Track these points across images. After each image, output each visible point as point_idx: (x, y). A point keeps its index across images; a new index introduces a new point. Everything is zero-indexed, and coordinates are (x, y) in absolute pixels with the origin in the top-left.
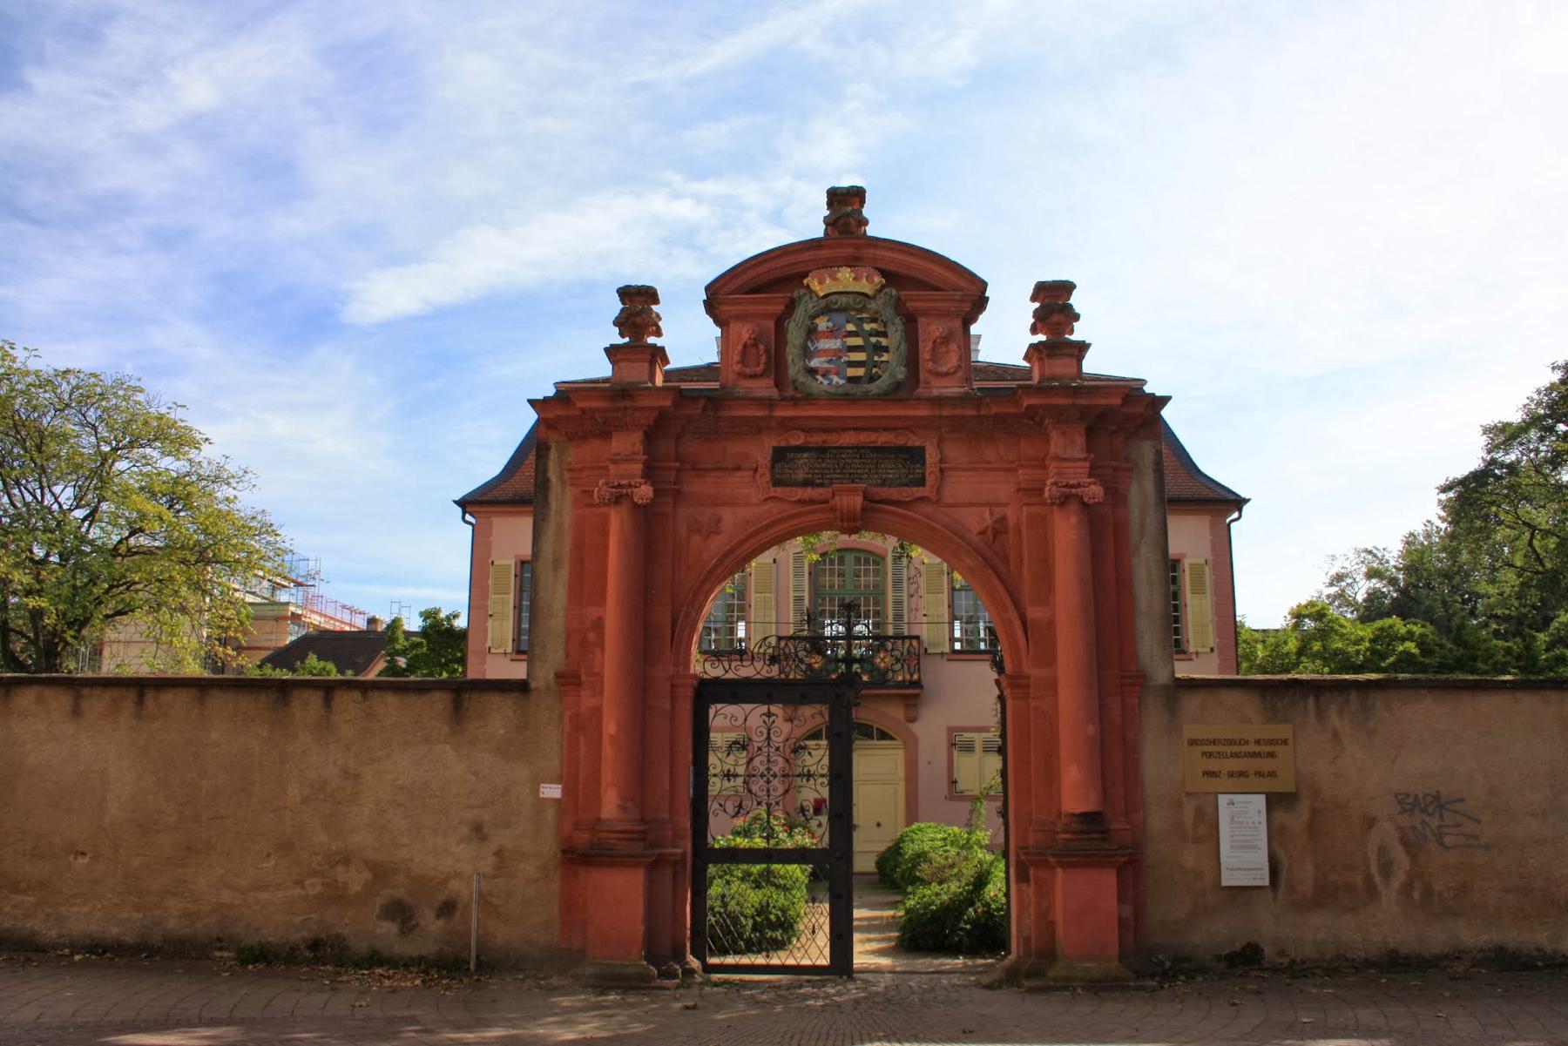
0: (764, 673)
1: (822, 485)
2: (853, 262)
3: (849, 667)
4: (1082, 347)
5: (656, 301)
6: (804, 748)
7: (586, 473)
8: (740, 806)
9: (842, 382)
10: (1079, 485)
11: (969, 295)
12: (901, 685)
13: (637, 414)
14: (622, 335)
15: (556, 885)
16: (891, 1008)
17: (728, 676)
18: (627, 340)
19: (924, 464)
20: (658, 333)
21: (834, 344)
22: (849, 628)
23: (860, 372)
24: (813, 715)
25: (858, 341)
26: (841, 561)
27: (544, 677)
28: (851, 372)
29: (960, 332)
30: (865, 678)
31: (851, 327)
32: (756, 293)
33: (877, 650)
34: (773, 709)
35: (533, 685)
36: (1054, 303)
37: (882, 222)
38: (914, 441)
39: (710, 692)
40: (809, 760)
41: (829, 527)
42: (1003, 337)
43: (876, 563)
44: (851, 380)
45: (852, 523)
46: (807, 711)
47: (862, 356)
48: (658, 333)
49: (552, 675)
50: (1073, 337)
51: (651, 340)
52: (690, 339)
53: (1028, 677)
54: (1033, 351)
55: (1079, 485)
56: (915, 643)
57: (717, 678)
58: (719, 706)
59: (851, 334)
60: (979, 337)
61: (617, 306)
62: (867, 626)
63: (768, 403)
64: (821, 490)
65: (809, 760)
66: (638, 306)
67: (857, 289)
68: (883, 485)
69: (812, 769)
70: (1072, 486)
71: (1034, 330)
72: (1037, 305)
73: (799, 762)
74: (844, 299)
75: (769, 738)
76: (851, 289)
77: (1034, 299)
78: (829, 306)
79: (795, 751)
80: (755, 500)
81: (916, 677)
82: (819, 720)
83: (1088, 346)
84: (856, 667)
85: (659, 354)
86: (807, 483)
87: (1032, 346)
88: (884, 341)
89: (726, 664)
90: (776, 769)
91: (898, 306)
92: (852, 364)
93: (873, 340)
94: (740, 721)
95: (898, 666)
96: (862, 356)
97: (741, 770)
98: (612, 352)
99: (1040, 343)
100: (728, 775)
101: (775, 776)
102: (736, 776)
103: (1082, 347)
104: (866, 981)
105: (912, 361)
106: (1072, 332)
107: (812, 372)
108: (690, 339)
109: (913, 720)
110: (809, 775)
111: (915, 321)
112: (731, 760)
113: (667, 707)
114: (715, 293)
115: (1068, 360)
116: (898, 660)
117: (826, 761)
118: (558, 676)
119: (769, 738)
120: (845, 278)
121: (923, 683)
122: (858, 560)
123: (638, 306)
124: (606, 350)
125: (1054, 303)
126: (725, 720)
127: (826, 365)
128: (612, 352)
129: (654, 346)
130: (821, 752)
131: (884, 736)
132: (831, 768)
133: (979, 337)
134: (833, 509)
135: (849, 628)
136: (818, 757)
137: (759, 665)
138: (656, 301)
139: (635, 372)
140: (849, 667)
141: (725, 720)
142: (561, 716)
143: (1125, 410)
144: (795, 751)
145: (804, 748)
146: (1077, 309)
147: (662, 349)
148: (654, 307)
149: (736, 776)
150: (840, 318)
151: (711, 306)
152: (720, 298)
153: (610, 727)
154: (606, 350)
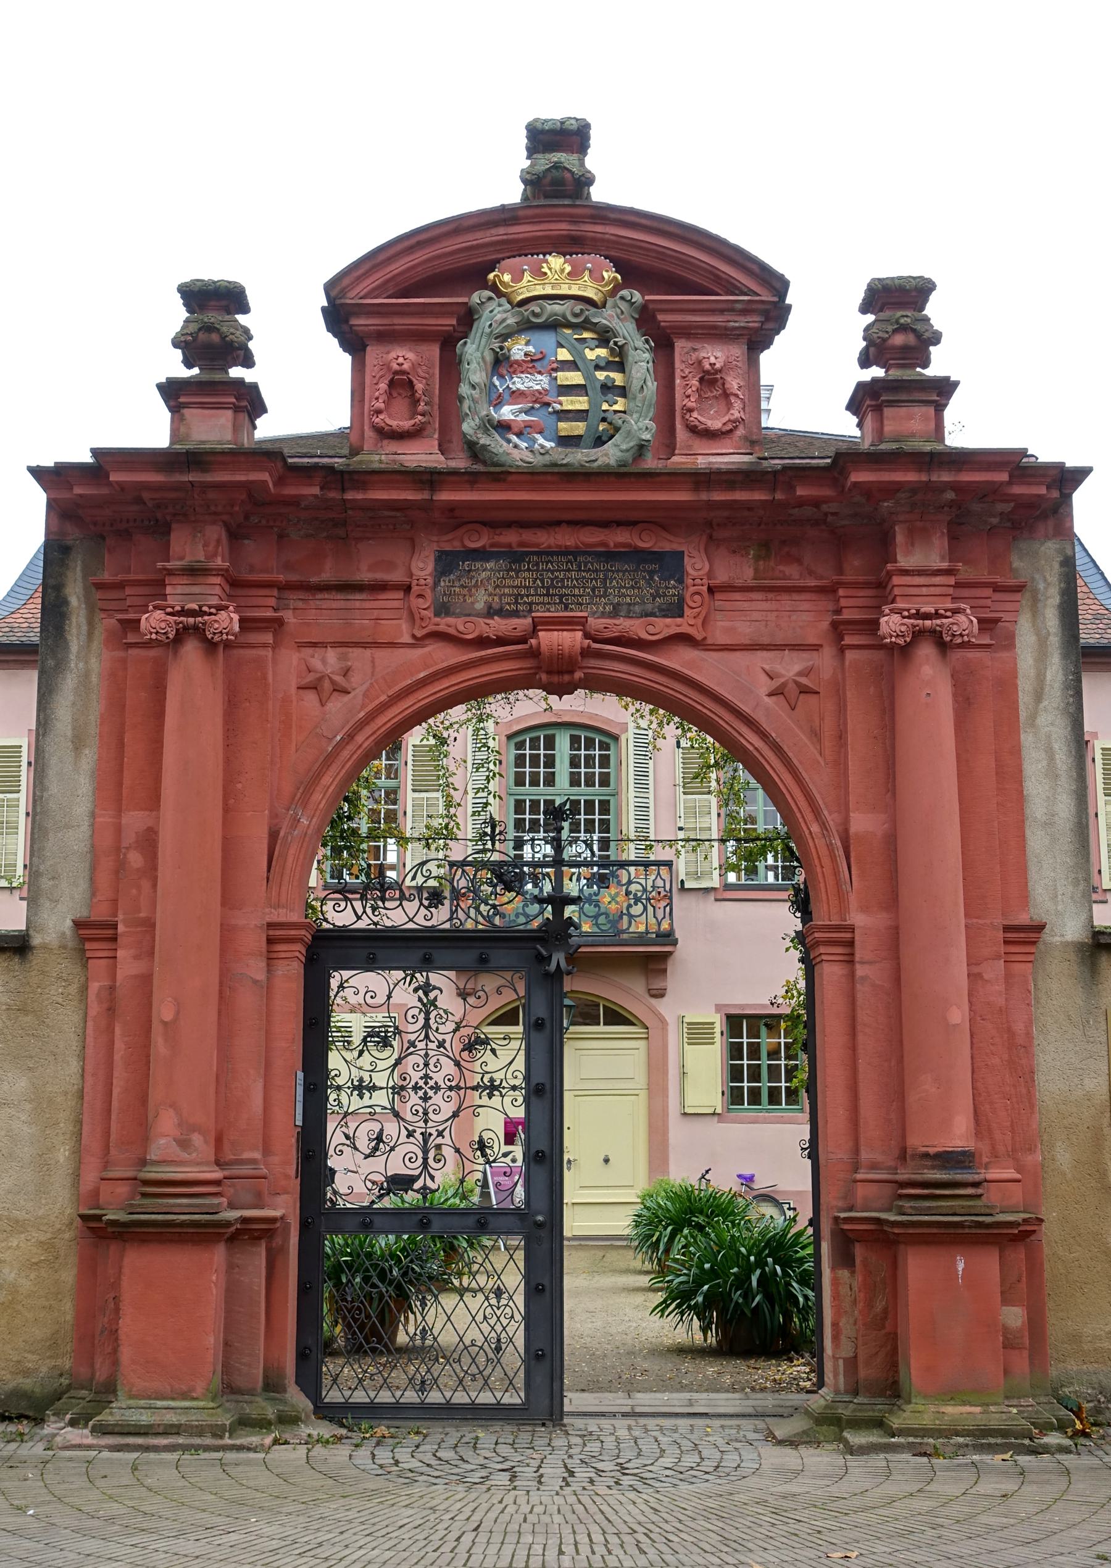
0: (420, 920)
1: (515, 614)
2: (569, 245)
3: (558, 911)
4: (945, 388)
5: (245, 309)
6: (486, 1042)
7: (128, 591)
8: (379, 1139)
9: (549, 445)
10: (937, 615)
11: (756, 304)
12: (641, 939)
13: (212, 495)
14: (188, 364)
15: (68, 1276)
16: (626, 1481)
17: (361, 925)
18: (196, 371)
19: (681, 581)
20: (248, 361)
21: (537, 382)
22: (558, 848)
23: (578, 428)
24: (501, 990)
25: (575, 378)
26: (550, 743)
27: (56, 925)
28: (566, 428)
29: (742, 364)
30: (586, 928)
31: (564, 355)
32: (411, 299)
33: (602, 881)
34: (435, 978)
35: (36, 940)
36: (898, 314)
37: (616, 179)
38: (667, 545)
39: (329, 951)
40: (493, 1064)
41: (525, 682)
42: (809, 386)
43: (604, 746)
44: (568, 441)
45: (559, 676)
46: (489, 982)
47: (580, 403)
48: (248, 361)
49: (69, 923)
50: (931, 372)
51: (236, 372)
52: (305, 389)
53: (851, 929)
54: (864, 401)
55: (937, 615)
56: (664, 871)
57: (344, 929)
58: (346, 974)
59: (565, 365)
60: (770, 388)
61: (177, 315)
62: (589, 846)
63: (429, 479)
64: (515, 621)
65: (493, 1064)
66: (214, 321)
67: (575, 291)
68: (615, 614)
69: (498, 1076)
70: (927, 616)
71: (865, 361)
72: (870, 318)
73: (477, 1066)
74: (557, 308)
75: (427, 1026)
76: (564, 290)
77: (865, 309)
78: (533, 320)
79: (469, 1047)
80: (407, 639)
81: (665, 926)
82: (509, 996)
83: (956, 384)
84: (569, 911)
85: (250, 402)
86: (490, 612)
87: (861, 387)
88: (618, 378)
89: (358, 905)
90: (414, 1099)
91: (645, 319)
92: (564, 415)
93: (601, 375)
94: (381, 999)
95: (637, 909)
96: (580, 403)
97: (380, 1079)
98: (171, 391)
99: (875, 381)
100: (361, 1088)
101: (436, 1088)
102: (374, 1088)
103: (945, 388)
104: (586, 1436)
105: (666, 411)
106: (926, 364)
107: (504, 427)
108: (305, 389)
109: (660, 994)
110: (492, 1088)
111: (671, 346)
112: (366, 1060)
113: (261, 976)
114: (343, 293)
115: (919, 411)
116: (637, 900)
117: (520, 1064)
118: (78, 924)
119: (427, 1026)
120: (556, 275)
121: (678, 934)
122: (575, 741)
123: (214, 321)
124: (160, 387)
125: (898, 314)
126: (363, 997)
127: (523, 417)
128: (171, 391)
129: (240, 382)
130: (515, 1044)
131: (616, 1017)
132: (527, 1078)
133: (770, 388)
134: (535, 653)
135: (558, 848)
136: (507, 1058)
137: (411, 907)
138: (245, 309)
139: (213, 429)
140: (558, 911)
141: (363, 997)
142: (84, 989)
143: (1017, 490)
144: (469, 1047)
145: (486, 1042)
146: (937, 324)
147: (254, 387)
148: (241, 319)
149: (374, 1088)
150: (547, 340)
151: (338, 317)
152: (348, 314)
153: (826, 813)
154: (160, 387)
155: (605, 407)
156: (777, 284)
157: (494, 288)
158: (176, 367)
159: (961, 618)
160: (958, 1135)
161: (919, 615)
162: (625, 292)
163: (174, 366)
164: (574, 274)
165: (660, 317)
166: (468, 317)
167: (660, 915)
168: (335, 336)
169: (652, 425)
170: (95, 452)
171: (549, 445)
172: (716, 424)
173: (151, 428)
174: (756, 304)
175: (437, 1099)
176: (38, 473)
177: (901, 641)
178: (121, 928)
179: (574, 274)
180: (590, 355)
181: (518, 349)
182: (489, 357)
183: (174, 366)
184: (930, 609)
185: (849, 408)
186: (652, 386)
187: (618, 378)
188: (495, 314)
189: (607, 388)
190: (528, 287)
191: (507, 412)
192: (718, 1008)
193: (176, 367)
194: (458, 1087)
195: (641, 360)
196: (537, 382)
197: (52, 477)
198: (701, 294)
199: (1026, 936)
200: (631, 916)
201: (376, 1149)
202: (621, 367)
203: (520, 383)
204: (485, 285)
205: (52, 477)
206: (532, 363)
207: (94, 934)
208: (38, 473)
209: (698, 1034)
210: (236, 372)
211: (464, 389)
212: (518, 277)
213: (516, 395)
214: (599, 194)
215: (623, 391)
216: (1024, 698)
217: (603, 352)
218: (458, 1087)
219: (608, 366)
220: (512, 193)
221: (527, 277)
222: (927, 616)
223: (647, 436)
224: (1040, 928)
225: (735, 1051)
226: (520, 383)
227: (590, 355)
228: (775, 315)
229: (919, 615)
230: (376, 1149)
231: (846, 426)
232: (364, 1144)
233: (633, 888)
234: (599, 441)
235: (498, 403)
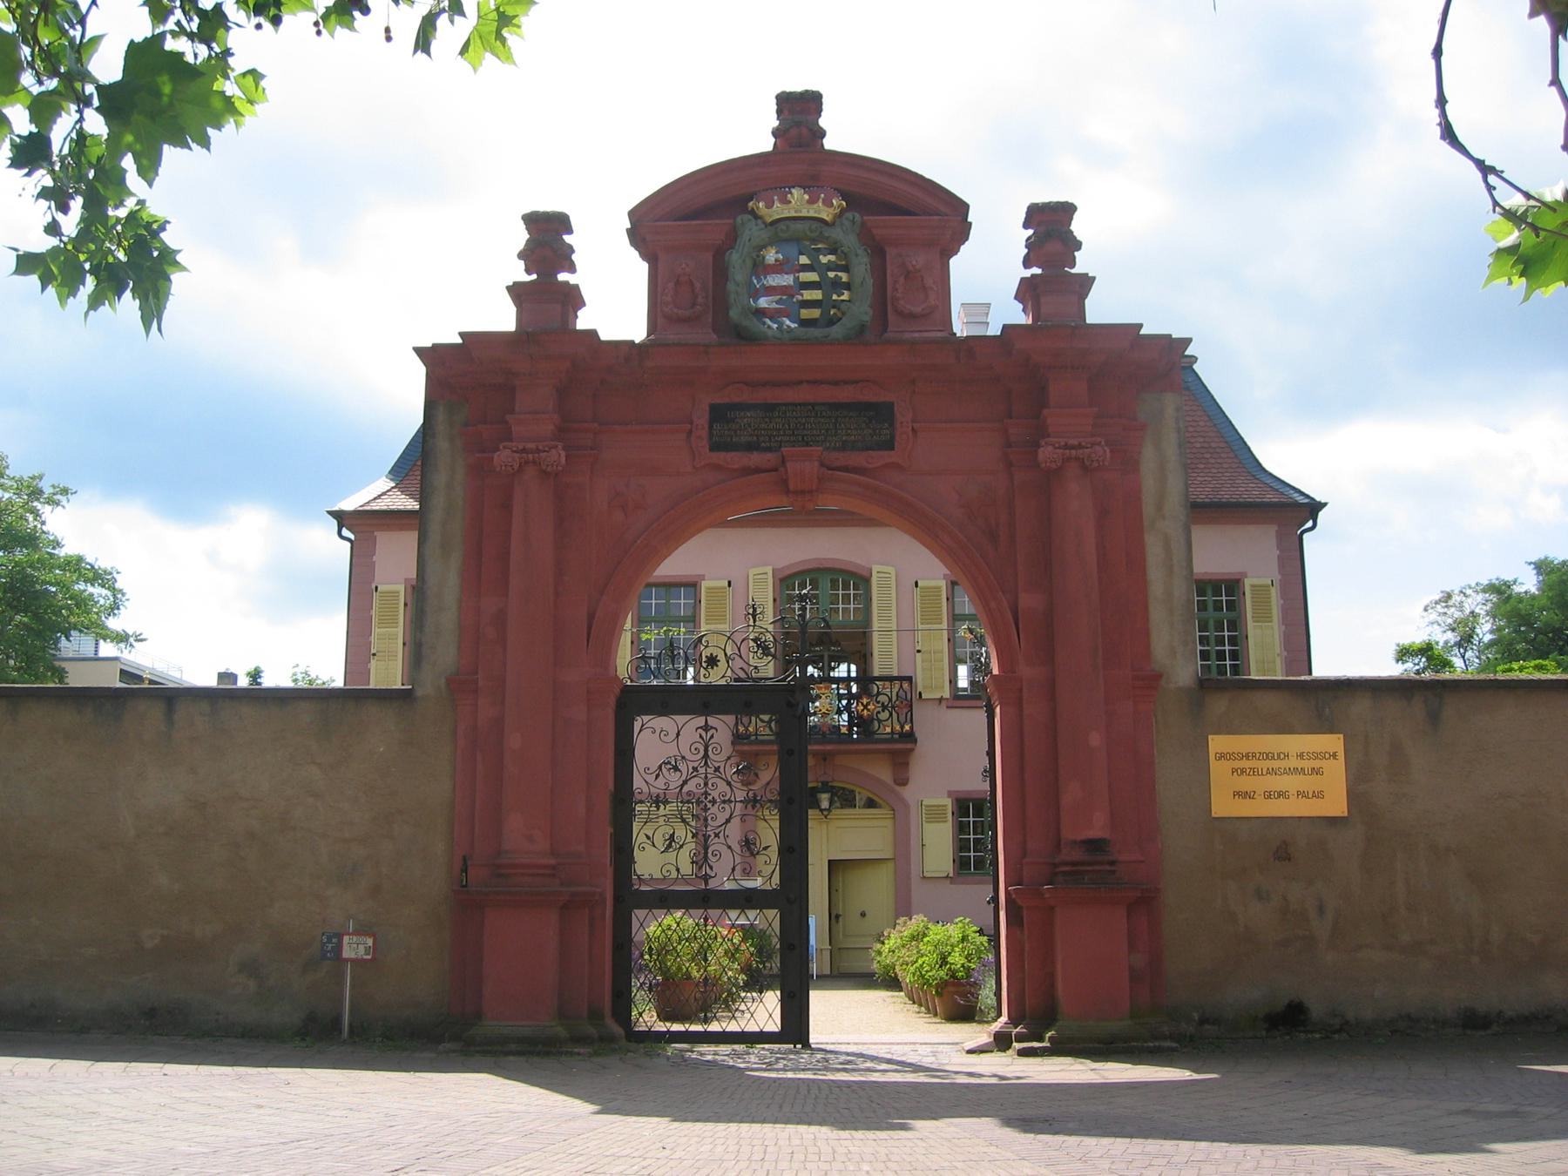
4: (1086, 282)
5: (570, 231)
9: (793, 325)
10: (1080, 446)
14: (528, 271)
18: (534, 277)
19: (892, 424)
21: (786, 280)
23: (815, 313)
25: (812, 277)
27: (431, 685)
28: (806, 313)
31: (804, 260)
34: (712, 721)
35: (419, 693)
36: (1050, 227)
37: (843, 132)
38: (883, 397)
44: (805, 323)
47: (816, 295)
48: (572, 268)
51: (562, 277)
52: (616, 300)
55: (1080, 446)
58: (646, 718)
59: (805, 268)
66: (547, 238)
67: (812, 214)
70: (1073, 447)
71: (1027, 263)
72: (1030, 232)
75: (706, 756)
76: (804, 214)
77: (1026, 226)
78: (782, 232)
88: (844, 277)
91: (865, 235)
93: (831, 274)
96: (816, 295)
98: (516, 291)
103: (1086, 282)
106: (1073, 265)
107: (761, 313)
116: (884, 708)
117: (776, 786)
120: (798, 202)
123: (547, 238)
124: (508, 288)
125: (1050, 227)
127: (774, 305)
128: (516, 291)
138: (570, 231)
147: (576, 287)
148: (567, 238)
154: (508, 288)
155: (835, 297)
156: (961, 208)
157: (753, 213)
158: (519, 273)
159: (1097, 448)
160: (1097, 829)
161: (1067, 447)
162: (849, 215)
163: (519, 273)
164: (812, 201)
165: (875, 231)
166: (732, 237)
167: (902, 718)
168: (644, 256)
169: (871, 312)
170: (462, 335)
171: (793, 325)
172: (918, 310)
173: (502, 318)
174: (938, 217)
175: (714, 810)
176: (419, 351)
177: (1054, 466)
178: (481, 683)
179: (812, 201)
180: (824, 260)
181: (771, 256)
182: (749, 263)
183: (519, 273)
184: (1074, 442)
185: (1016, 298)
186: (870, 282)
187: (844, 277)
188: (751, 232)
189: (837, 285)
190: (778, 211)
191: (763, 302)
192: (950, 794)
193: (519, 273)
194: (730, 801)
195: (862, 265)
196: (786, 280)
197: (432, 356)
198: (908, 216)
199: (1150, 681)
200: (880, 721)
201: (670, 846)
202: (846, 269)
203: (774, 280)
204: (745, 210)
205: (432, 356)
206: (778, 268)
207: (461, 685)
208: (419, 351)
209: (935, 815)
210: (562, 277)
211: (731, 286)
212: (770, 205)
213: (770, 290)
214: (829, 143)
215: (848, 286)
216: (1148, 509)
217: (832, 258)
218: (730, 801)
219: (837, 268)
220: (766, 144)
221: (777, 204)
222: (1073, 447)
223: (867, 318)
224: (1158, 677)
225: (961, 828)
226: (774, 280)
227: (824, 260)
228: (961, 231)
229: (1067, 447)
230: (670, 846)
231: (1017, 315)
232: (659, 841)
233: (882, 698)
234: (831, 322)
235: (756, 295)
